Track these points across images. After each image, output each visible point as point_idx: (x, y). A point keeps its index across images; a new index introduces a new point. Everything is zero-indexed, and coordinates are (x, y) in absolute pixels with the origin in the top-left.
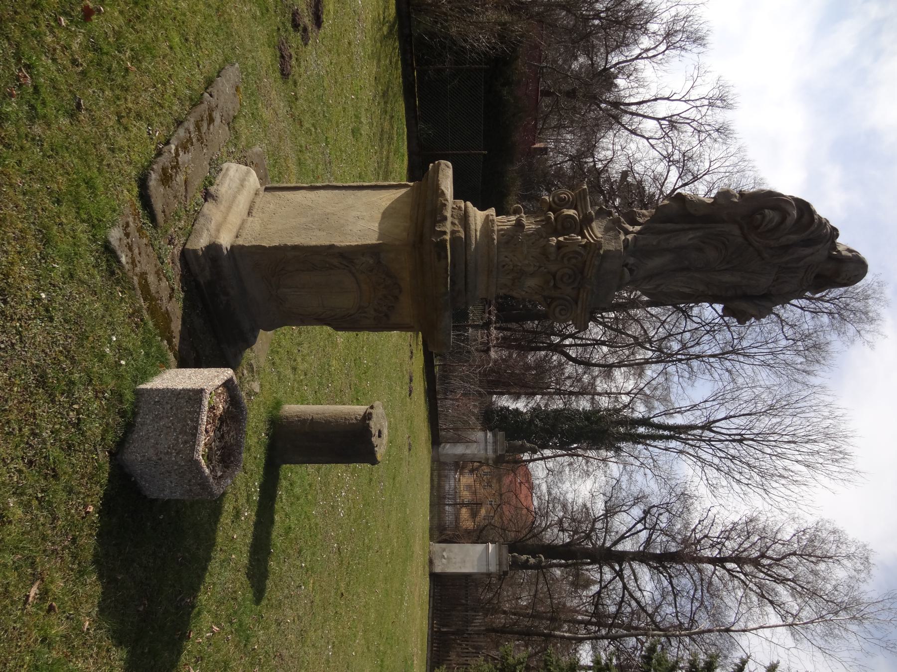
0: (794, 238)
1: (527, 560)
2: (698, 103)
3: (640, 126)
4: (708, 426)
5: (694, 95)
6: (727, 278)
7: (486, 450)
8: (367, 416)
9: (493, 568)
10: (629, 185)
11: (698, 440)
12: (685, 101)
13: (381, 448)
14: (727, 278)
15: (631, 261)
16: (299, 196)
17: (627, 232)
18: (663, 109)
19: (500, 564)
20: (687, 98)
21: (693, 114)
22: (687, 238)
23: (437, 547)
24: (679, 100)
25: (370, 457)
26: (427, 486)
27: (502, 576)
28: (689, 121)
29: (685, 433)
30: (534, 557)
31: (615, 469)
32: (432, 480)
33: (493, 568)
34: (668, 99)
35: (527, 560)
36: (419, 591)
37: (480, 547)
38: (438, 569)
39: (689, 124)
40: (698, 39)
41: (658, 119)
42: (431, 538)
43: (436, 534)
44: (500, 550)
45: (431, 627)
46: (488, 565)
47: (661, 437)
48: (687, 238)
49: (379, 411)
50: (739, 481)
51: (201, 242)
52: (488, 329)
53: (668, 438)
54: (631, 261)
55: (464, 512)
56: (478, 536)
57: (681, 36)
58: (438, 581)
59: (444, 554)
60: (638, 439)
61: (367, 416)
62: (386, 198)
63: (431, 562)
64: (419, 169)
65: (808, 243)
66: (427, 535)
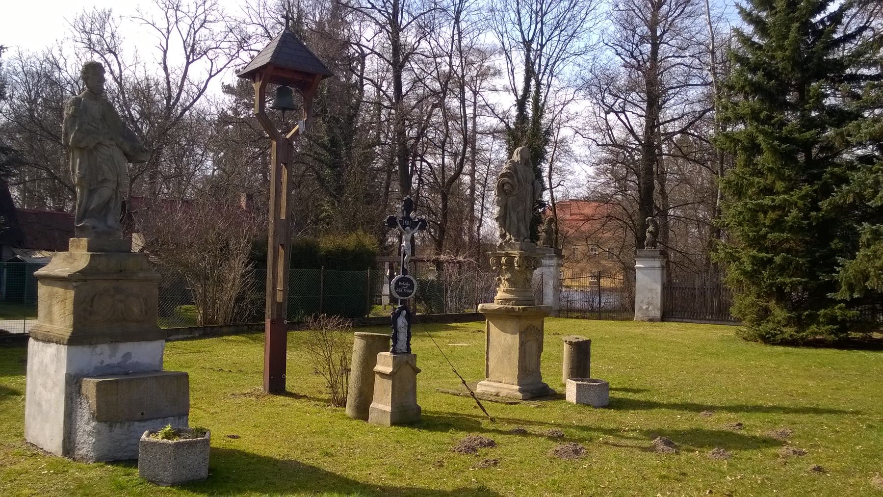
0: (516, 180)
1: (651, 232)
2: (173, 20)
3: (196, 83)
4: (527, 44)
5: (163, 25)
6: (528, 202)
7: (550, 266)
8: (570, 343)
9: (657, 263)
10: (240, 84)
11: (541, 55)
12: (169, 33)
13: (582, 338)
14: (528, 202)
15: (522, 238)
16: (491, 364)
17: (510, 239)
18: (177, 59)
19: (654, 257)
20: (164, 31)
21: (184, 26)
22: (514, 218)
23: (638, 314)
24: (167, 40)
25: (587, 343)
26: (584, 321)
27: (664, 254)
28: (193, 31)
29: (533, 64)
30: (648, 226)
31: (565, 132)
32: (577, 318)
33: (657, 263)
34: (165, 52)
35: (651, 232)
36: (674, 330)
37: (639, 275)
38: (658, 314)
39: (195, 32)
40: (105, 18)
41: (188, 63)
42: (631, 319)
43: (625, 315)
44: (641, 257)
45: (709, 321)
46: (654, 268)
47: (538, 92)
48: (514, 218)
49: (568, 339)
50: (583, 20)
51: (520, 395)
52: (442, 262)
53: (538, 84)
54: (522, 238)
55: (605, 282)
56: (629, 271)
57: (96, 31)
58: (668, 314)
59: (644, 307)
60: (539, 110)
61: (570, 343)
62: (494, 330)
63: (651, 320)
64: (478, 317)
65: (516, 172)
66: (627, 323)
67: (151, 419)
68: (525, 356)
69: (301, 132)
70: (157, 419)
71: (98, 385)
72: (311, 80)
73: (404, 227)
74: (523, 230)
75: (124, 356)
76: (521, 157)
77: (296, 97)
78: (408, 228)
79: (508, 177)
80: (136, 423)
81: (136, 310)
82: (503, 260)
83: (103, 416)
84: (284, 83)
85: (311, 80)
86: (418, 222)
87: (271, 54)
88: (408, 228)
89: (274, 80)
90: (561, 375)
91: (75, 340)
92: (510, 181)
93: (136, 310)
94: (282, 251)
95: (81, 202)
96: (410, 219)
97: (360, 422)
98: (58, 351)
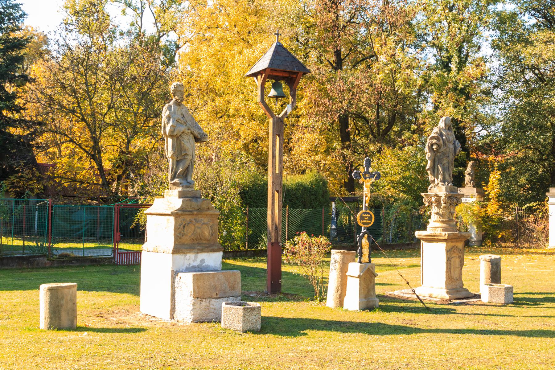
67: (221, 298)
68: (450, 268)
69: (288, 113)
70: (224, 298)
71: (194, 275)
72: (295, 76)
73: (365, 178)
74: (447, 177)
75: (201, 261)
76: (445, 124)
77: (286, 89)
78: (368, 179)
79: (436, 139)
80: (213, 300)
81: (207, 233)
82: (433, 200)
83: (199, 296)
84: (277, 79)
85: (295, 76)
86: (374, 175)
87: (268, 61)
88: (368, 179)
89: (270, 77)
90: (478, 280)
91: (177, 250)
92: (437, 143)
93: (207, 233)
94: (277, 195)
95: (173, 168)
96: (369, 173)
97: (341, 308)
98: (552, 203)
